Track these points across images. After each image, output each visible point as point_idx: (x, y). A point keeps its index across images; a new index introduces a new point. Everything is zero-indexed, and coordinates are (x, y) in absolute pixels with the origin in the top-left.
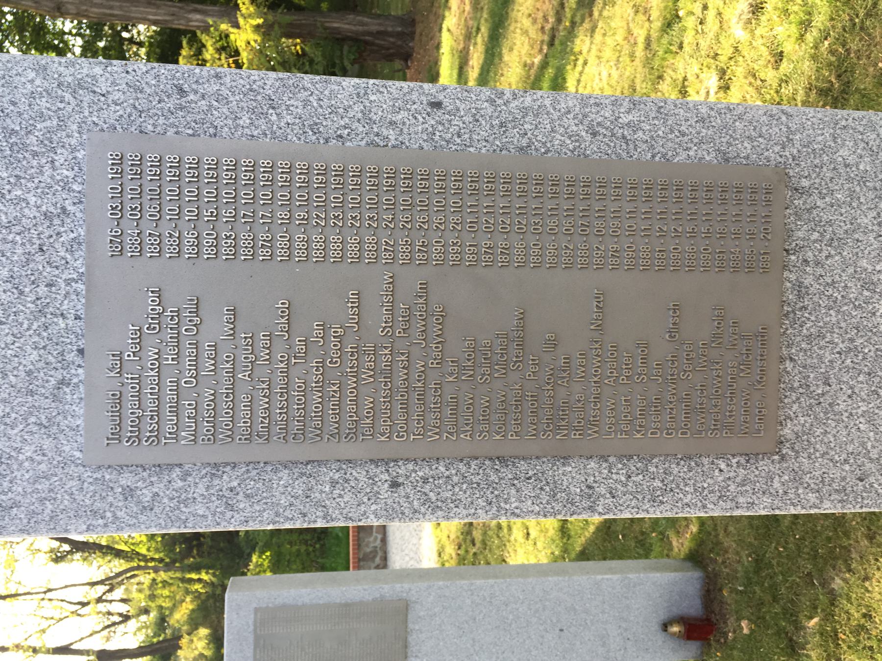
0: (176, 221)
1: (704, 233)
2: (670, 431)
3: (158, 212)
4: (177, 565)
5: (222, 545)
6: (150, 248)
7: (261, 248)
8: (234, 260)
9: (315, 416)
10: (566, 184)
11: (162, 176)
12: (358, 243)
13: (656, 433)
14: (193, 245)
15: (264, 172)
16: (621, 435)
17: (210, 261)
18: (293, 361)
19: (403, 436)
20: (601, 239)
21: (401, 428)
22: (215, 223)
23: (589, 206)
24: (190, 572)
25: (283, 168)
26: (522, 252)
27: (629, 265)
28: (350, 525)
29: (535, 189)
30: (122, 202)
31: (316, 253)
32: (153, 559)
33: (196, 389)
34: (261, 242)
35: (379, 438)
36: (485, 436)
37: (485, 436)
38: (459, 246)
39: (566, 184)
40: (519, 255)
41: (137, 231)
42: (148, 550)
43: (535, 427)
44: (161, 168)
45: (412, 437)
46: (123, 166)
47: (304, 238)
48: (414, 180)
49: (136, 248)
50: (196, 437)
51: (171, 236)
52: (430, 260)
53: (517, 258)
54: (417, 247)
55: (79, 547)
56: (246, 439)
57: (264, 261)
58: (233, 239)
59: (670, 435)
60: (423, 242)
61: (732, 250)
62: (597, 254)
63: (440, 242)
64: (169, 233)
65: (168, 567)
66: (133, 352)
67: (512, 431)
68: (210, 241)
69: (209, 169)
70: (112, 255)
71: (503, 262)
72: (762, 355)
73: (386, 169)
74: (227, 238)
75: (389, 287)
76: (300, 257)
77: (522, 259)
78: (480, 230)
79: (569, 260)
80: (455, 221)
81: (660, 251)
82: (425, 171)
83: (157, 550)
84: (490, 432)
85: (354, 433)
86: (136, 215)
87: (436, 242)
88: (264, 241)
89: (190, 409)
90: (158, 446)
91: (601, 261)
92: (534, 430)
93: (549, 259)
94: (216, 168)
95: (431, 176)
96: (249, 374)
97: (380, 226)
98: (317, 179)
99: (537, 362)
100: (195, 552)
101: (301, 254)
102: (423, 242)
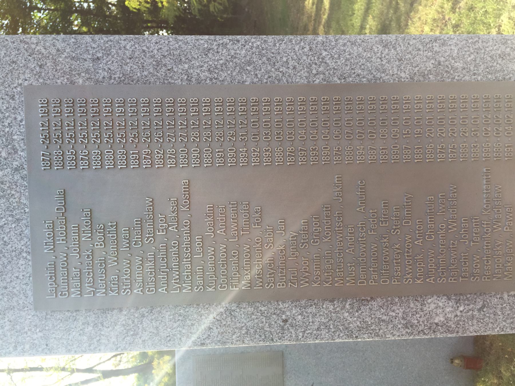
6: (107, 163)
11: (113, 113)
12: (282, 152)
15: (229, 106)
18: (242, 233)
19: (152, 290)
23: (317, 118)
25: (206, 103)
27: (395, 159)
30: (49, 132)
34: (168, 155)
38: (317, 151)
40: (349, 155)
41: (245, 149)
45: (461, 279)
46: (49, 108)
49: (281, 159)
54: (334, 152)
58: (270, 152)
60: (338, 148)
64: (157, 151)
69: (144, 106)
71: (325, 161)
73: (192, 100)
75: (150, 209)
80: (464, 130)
85: (129, 289)
86: (280, 138)
87: (324, 148)
88: (171, 154)
89: (328, 264)
95: (236, 102)
97: (237, 139)
98: (143, 110)
101: (134, 163)
102: (338, 148)
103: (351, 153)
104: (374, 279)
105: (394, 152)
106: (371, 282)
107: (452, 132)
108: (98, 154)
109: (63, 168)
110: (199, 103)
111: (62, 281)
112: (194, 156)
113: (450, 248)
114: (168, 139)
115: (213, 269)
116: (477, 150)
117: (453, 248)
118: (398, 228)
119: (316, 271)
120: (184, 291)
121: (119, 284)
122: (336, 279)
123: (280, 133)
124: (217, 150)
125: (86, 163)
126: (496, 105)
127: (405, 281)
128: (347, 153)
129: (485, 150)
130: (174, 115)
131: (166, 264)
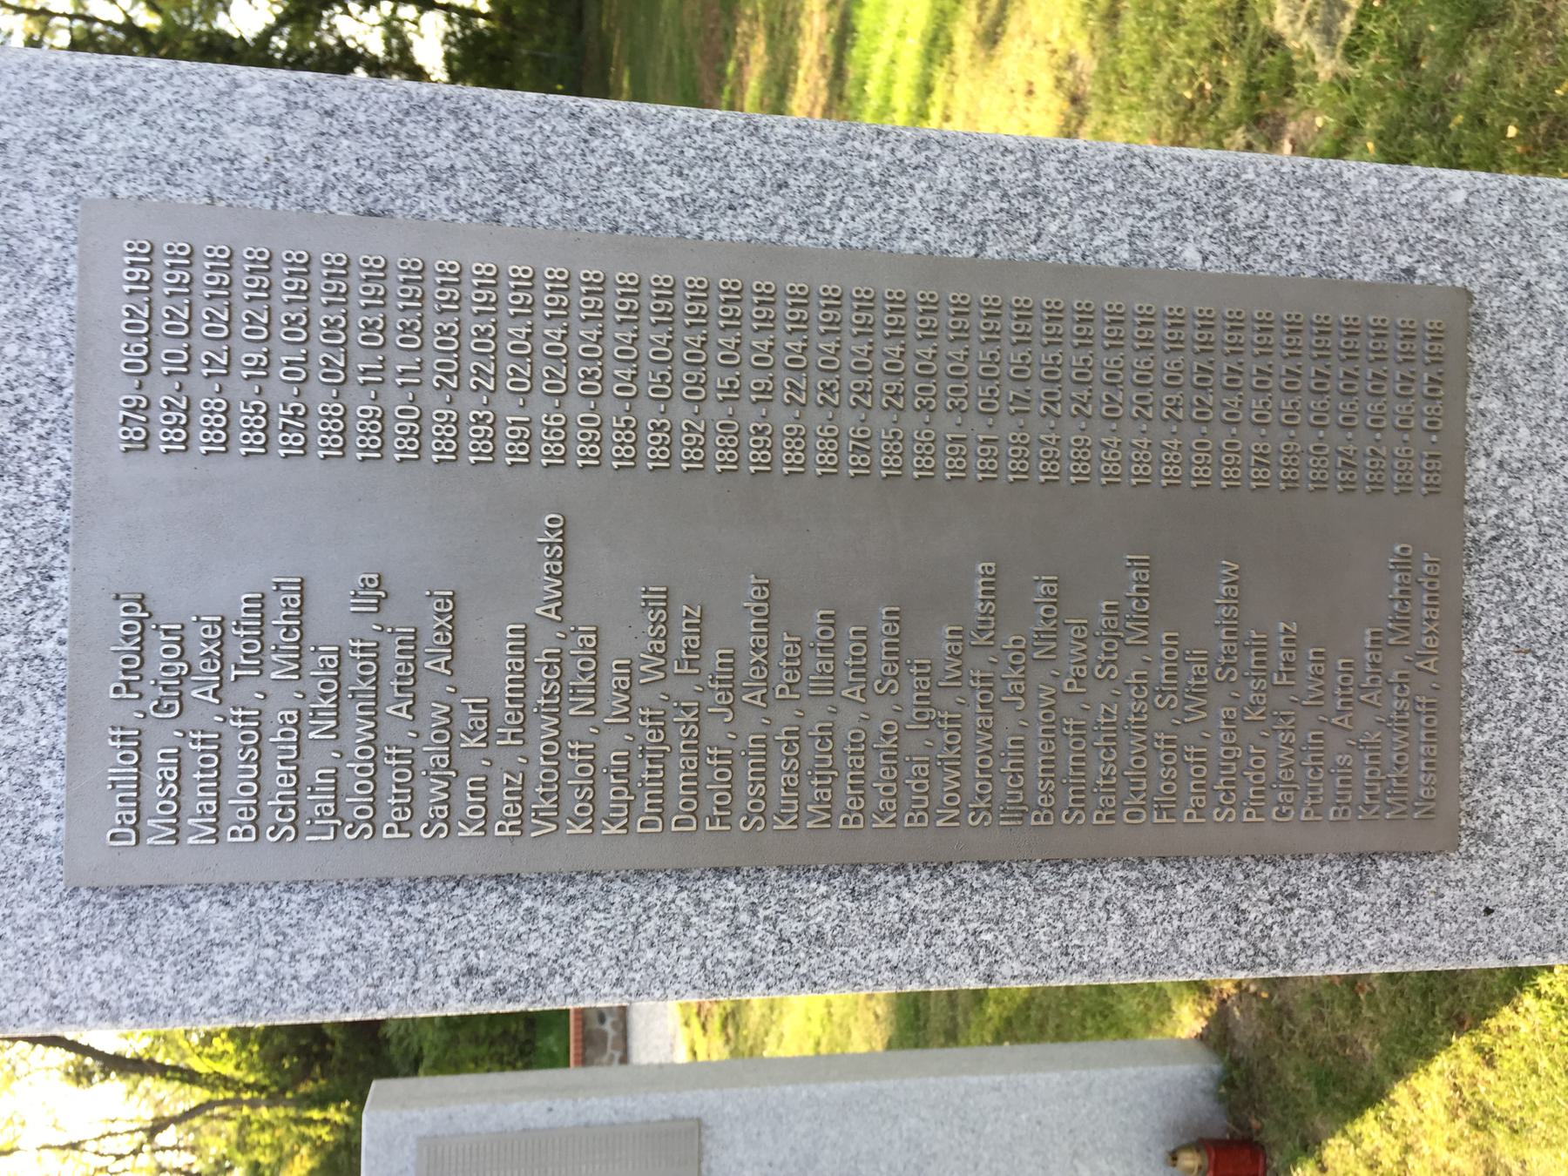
0: (181, 378)
1: (722, 390)
2: (1284, 809)
3: (145, 358)
4: (289, 1095)
5: (361, 1058)
6: (324, 441)
7: (283, 430)
8: (143, 454)
9: (650, 780)
10: (756, 299)
13: (1138, 815)
14: (176, 425)
16: (1159, 817)
17: (252, 460)
20: (990, 421)
21: (359, 812)
22: (263, 383)
24: (309, 1108)
25: (445, 274)
26: (731, 441)
28: (570, 1007)
29: (922, 321)
31: (547, 449)
32: (248, 1087)
33: (180, 723)
35: (461, 830)
36: (757, 823)
37: (757, 823)
39: (756, 299)
42: (237, 1067)
43: (990, 737)
44: (153, 268)
46: (195, 270)
47: (375, 412)
48: (571, 293)
49: (257, 438)
50: (178, 831)
51: (170, 406)
52: (709, 461)
53: (618, 451)
54: (1254, 457)
55: (116, 1064)
56: (512, 828)
57: (587, 470)
58: (491, 425)
59: (1285, 815)
61: (1165, 443)
62: (687, 439)
63: (593, 420)
65: (273, 1101)
66: (398, 823)
67: (389, 821)
68: (408, 425)
70: (127, 450)
72: (1227, 656)
74: (479, 421)
76: (404, 451)
77: (831, 459)
78: (642, 395)
79: (991, 464)
81: (1431, 457)
82: (734, 284)
83: (252, 1068)
84: (768, 814)
86: (595, 388)
88: (1261, 455)
90: (376, 839)
91: (991, 464)
92: (956, 779)
93: (687, 454)
94: (150, 263)
96: (215, 691)
99: (928, 669)
100: (317, 1070)
101: (131, 436)
103: (928, 448)
104: (1196, 808)
105: (1198, 458)
106: (1249, 815)
107: (446, 375)
108: (448, 422)
109: (146, 448)
110: (536, 281)
111: (648, 801)
112: (583, 435)
113: (1098, 723)
114: (476, 383)
115: (289, 780)
116: (896, 447)
117: (1136, 723)
118: (1113, 662)
119: (754, 783)
120: (150, 841)
121: (559, 820)
122: (810, 808)
123: (594, 373)
124: (509, 419)
125: (296, 439)
126: (1079, 330)
127: (974, 819)
128: (822, 444)
129: (1014, 452)
130: (150, 291)
131: (371, 765)
